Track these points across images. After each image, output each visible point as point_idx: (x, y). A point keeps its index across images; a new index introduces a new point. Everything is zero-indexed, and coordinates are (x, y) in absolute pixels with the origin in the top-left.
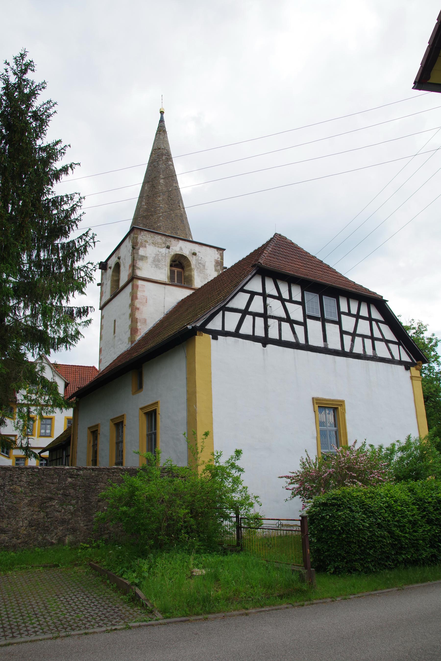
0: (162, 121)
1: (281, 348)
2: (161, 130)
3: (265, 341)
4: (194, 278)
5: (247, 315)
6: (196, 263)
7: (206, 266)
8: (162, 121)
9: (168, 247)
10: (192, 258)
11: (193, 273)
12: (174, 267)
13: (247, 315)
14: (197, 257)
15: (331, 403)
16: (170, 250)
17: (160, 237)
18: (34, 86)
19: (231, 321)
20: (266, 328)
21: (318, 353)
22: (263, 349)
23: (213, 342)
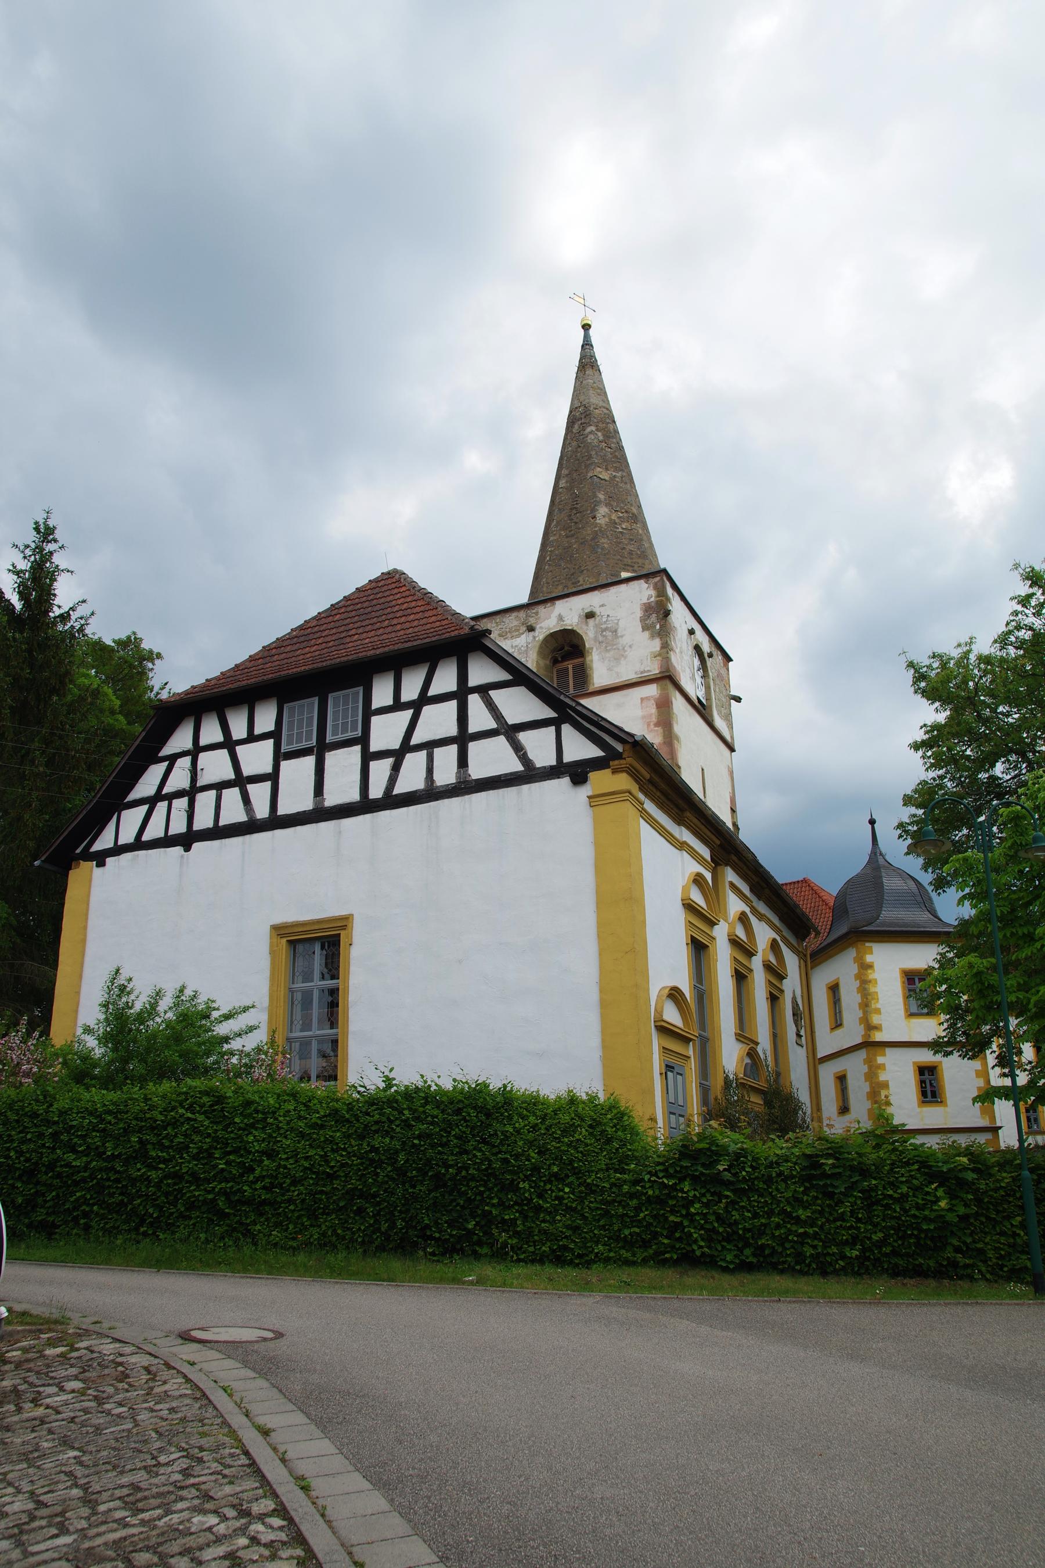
0: (587, 344)
1: (216, 844)
2: (588, 363)
3: (187, 840)
4: (591, 668)
5: (371, 763)
6: (596, 632)
7: (619, 631)
8: (587, 344)
9: (531, 629)
10: (585, 627)
11: (588, 659)
12: (562, 662)
13: (371, 763)
14: (598, 619)
15: (317, 927)
16: (536, 633)
17: (514, 614)
18: (42, 526)
19: (130, 821)
20: (246, 800)
21: (299, 828)
22: (182, 856)
23: (97, 872)
